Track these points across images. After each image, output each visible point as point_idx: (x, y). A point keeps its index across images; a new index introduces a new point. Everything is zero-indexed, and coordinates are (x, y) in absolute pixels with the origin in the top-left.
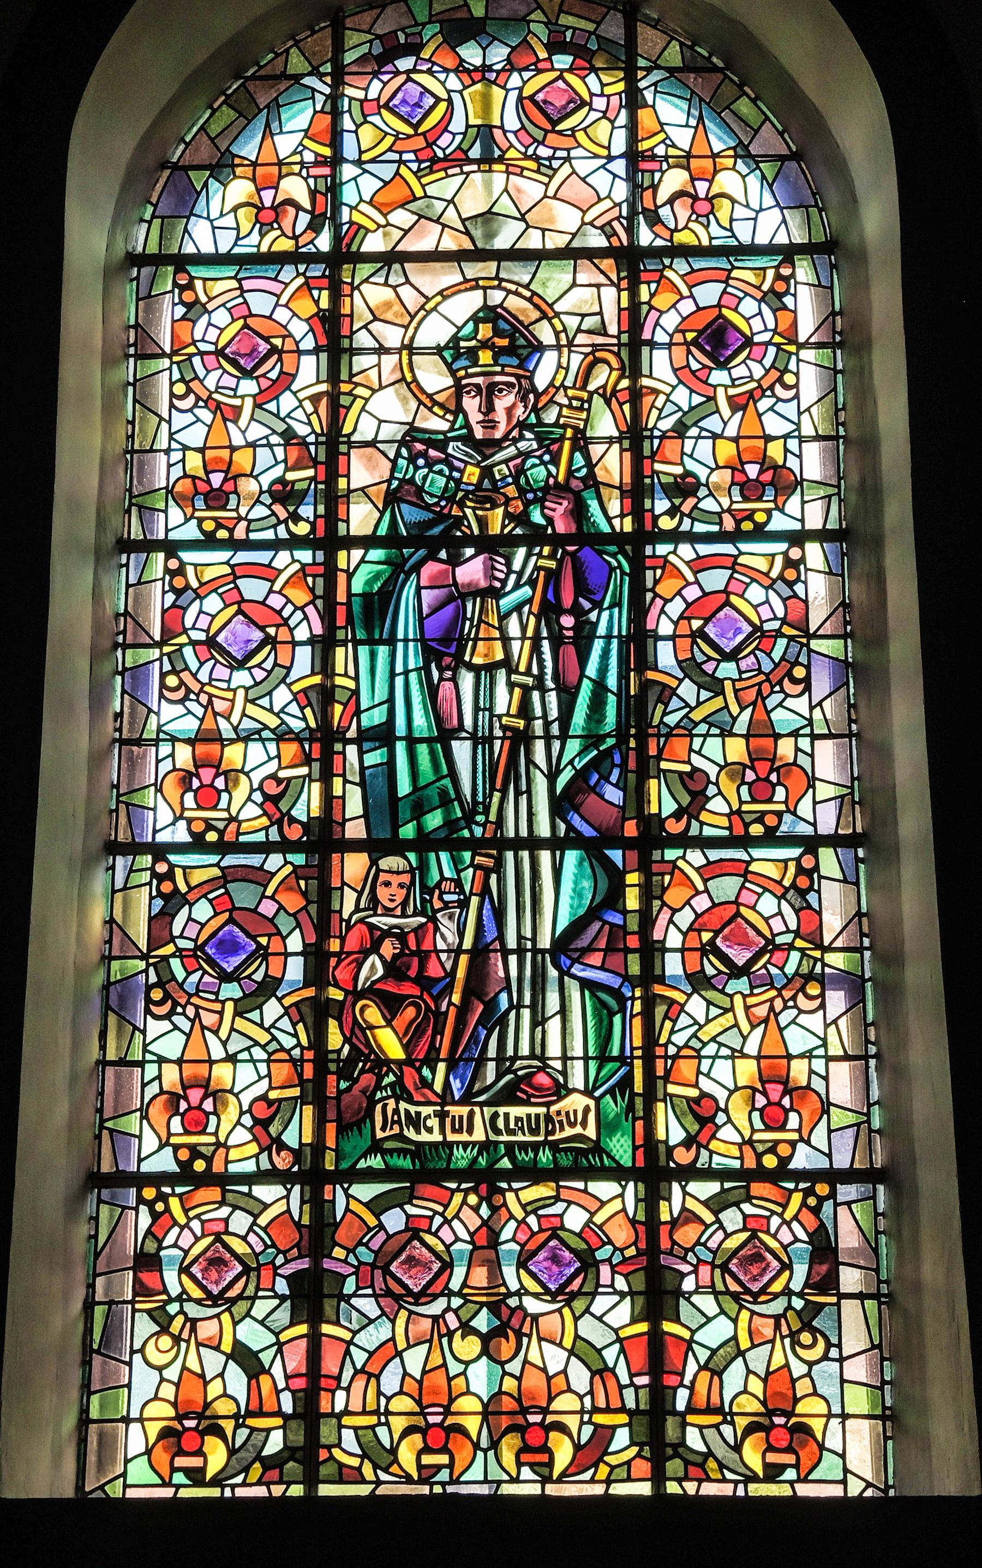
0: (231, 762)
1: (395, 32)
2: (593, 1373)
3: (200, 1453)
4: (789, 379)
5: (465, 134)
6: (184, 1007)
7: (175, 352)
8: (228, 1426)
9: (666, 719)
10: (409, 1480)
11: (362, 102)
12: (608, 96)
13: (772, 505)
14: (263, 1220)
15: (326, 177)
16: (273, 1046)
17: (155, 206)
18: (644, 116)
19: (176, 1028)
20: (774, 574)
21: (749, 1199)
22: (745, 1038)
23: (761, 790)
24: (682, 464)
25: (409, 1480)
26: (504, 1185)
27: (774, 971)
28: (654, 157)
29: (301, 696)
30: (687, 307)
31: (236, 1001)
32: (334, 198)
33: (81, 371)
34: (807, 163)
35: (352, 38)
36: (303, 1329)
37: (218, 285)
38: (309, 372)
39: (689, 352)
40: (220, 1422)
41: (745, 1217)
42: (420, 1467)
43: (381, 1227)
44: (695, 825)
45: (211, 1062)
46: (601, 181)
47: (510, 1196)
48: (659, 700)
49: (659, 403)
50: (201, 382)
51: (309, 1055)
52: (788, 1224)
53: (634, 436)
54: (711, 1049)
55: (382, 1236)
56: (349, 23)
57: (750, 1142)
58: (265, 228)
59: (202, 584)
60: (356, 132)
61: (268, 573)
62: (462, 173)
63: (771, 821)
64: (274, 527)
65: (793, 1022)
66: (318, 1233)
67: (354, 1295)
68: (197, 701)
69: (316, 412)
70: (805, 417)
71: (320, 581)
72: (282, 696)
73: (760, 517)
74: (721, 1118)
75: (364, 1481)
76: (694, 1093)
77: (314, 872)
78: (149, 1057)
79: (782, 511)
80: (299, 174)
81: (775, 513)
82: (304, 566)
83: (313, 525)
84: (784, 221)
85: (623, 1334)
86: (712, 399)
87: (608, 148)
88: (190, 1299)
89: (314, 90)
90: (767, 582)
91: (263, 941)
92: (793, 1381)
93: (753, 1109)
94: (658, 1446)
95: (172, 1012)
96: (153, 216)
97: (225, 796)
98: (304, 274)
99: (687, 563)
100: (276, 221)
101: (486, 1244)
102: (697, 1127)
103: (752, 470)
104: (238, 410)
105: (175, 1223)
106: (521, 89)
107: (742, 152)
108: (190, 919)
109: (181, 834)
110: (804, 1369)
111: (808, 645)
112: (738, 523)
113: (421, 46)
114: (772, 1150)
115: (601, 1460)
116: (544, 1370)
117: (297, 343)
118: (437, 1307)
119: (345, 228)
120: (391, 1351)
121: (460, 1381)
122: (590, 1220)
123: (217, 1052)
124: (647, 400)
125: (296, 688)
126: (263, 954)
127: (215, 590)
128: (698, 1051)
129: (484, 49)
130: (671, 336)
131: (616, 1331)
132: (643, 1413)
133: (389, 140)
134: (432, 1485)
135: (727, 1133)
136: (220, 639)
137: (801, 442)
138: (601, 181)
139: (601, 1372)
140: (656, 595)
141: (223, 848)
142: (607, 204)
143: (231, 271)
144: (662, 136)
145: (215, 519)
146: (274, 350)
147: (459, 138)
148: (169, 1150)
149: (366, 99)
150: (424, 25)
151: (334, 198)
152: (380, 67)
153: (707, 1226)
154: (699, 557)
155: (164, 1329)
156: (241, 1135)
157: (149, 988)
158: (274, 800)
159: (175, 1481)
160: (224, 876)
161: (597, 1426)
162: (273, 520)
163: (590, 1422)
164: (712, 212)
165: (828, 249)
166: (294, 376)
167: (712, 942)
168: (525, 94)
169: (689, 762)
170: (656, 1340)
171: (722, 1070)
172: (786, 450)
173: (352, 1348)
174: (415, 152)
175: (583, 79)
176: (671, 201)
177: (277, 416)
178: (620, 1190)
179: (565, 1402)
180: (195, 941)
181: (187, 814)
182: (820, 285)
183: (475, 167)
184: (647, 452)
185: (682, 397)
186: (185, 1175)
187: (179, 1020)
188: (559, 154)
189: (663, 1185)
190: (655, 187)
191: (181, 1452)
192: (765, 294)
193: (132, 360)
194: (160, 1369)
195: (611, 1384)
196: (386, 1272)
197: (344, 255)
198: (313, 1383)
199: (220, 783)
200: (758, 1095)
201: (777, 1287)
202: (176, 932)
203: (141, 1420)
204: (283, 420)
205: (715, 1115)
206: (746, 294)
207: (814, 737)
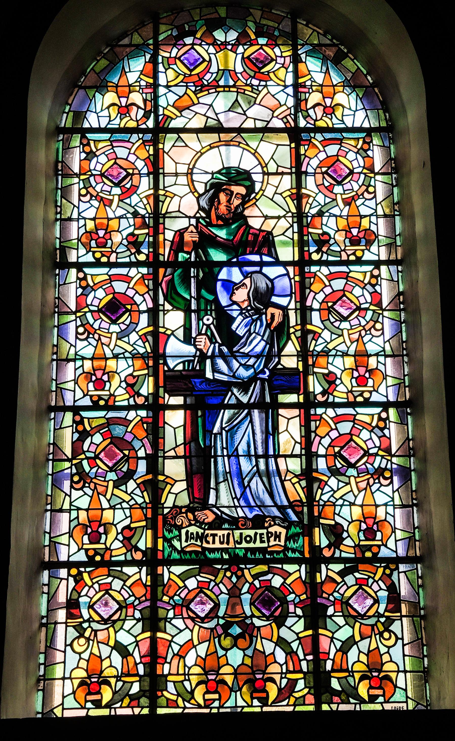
1: (183, 25)
2: (287, 654)
3: (99, 693)
5: (217, 73)
6: (89, 484)
7: (77, 311)
8: (113, 681)
9: (316, 348)
10: (199, 706)
12: (285, 57)
13: (364, 248)
14: (128, 583)
16: (132, 502)
17: (71, 105)
18: (301, 66)
19: (85, 494)
21: (358, 571)
22: (356, 497)
23: (361, 381)
24: (322, 229)
25: (199, 706)
27: (369, 466)
28: (305, 86)
29: (142, 486)
30: (322, 156)
31: (114, 481)
33: (37, 180)
34: (377, 91)
35: (163, 28)
36: (148, 634)
38: (145, 185)
39: (324, 177)
41: (357, 579)
42: (205, 700)
43: (185, 587)
44: (337, 552)
45: (103, 510)
46: (282, 97)
47: (246, 571)
49: (310, 201)
51: (149, 506)
52: (377, 582)
54: (340, 502)
55: (186, 591)
57: (351, 392)
58: (122, 116)
59: (92, 428)
60: (165, 72)
61: (126, 279)
62: (216, 92)
63: (375, 550)
65: (378, 490)
69: (148, 203)
70: (379, 206)
71: (151, 282)
72: (134, 337)
73: (359, 254)
75: (178, 707)
76: (326, 371)
79: (377, 391)
80: (139, 92)
82: (143, 275)
83: (147, 256)
84: (367, 116)
85: (301, 635)
87: (284, 81)
88: (94, 621)
90: (362, 285)
91: (126, 452)
92: (381, 655)
95: (84, 486)
96: (70, 111)
97: (108, 384)
98: (142, 139)
100: (128, 113)
101: (234, 593)
102: (328, 386)
103: (355, 232)
104: (111, 201)
105: (86, 585)
106: (243, 53)
107: (347, 84)
108: (92, 443)
109: (87, 402)
110: (386, 650)
111: (382, 314)
113: (196, 32)
114: (361, 395)
117: (139, 171)
118: (212, 624)
119: (161, 118)
120: (190, 645)
122: (284, 582)
123: (105, 505)
124: (304, 201)
125: (140, 333)
126: (127, 459)
127: (101, 287)
129: (226, 33)
130: (315, 170)
131: (297, 634)
132: (310, 673)
133: (181, 77)
134: (211, 708)
135: (341, 388)
137: (377, 218)
139: (290, 653)
140: (316, 435)
141: (108, 408)
142: (284, 108)
143: (107, 136)
144: (309, 77)
145: (101, 252)
146: (128, 174)
147: (214, 75)
149: (170, 57)
152: (177, 42)
153: (338, 584)
154: (331, 273)
155: (81, 635)
156: (117, 544)
157: (72, 476)
160: (108, 423)
161: (289, 679)
163: (285, 677)
165: (389, 131)
166: (138, 187)
167: (339, 452)
168: (245, 56)
169: (334, 520)
173: (172, 644)
174: (193, 83)
175: (273, 49)
176: (314, 107)
177: (130, 205)
178: (298, 568)
179: (273, 668)
180: (95, 453)
181: (85, 547)
182: (384, 146)
183: (222, 89)
184: (305, 223)
185: (321, 198)
186: (91, 562)
187: (87, 490)
188: (263, 83)
190: (306, 100)
191: (89, 693)
192: (359, 150)
193: (51, 462)
194: (80, 654)
195: (295, 658)
196: (188, 608)
197: (161, 130)
198: (154, 657)
199: (105, 378)
200: (362, 524)
201: (371, 613)
202: (85, 448)
203: (70, 678)
204: (133, 207)
205: (335, 380)
206: (350, 150)
207: (377, 216)
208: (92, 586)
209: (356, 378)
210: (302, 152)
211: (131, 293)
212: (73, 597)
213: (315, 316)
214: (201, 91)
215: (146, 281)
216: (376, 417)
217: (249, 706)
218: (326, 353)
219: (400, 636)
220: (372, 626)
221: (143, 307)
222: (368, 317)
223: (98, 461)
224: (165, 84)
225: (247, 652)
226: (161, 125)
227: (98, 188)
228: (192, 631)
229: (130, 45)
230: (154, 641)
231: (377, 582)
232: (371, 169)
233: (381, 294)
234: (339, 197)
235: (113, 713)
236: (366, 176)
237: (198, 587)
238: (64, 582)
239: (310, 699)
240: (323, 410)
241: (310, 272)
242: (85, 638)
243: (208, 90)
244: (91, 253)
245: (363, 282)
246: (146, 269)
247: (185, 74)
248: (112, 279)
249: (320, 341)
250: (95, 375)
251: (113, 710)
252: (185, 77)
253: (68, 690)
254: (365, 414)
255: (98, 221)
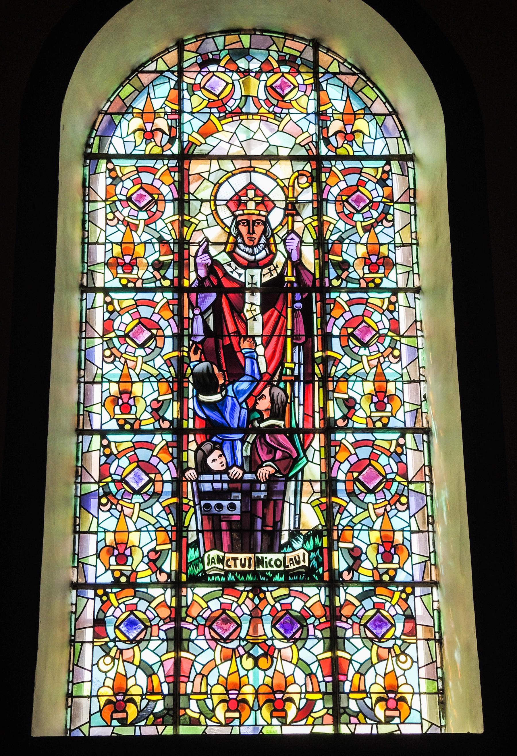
0: (138, 253)
1: (207, 53)
2: (306, 675)
3: (124, 711)
4: (390, 217)
5: (241, 99)
9: (336, 374)
11: (192, 85)
14: (153, 605)
15: (176, 119)
16: (158, 525)
20: (385, 307)
21: (376, 595)
22: (374, 522)
23: (380, 407)
24: (342, 256)
25: (222, 725)
26: (265, 589)
29: (166, 508)
32: (180, 129)
36: (172, 655)
37: (127, 166)
38: (170, 209)
39: (344, 206)
40: (133, 697)
43: (208, 607)
46: (304, 124)
47: (268, 594)
48: (333, 365)
49: (331, 228)
50: (120, 212)
52: (394, 606)
53: (320, 243)
54: (358, 527)
55: (209, 612)
56: (186, 48)
57: (370, 417)
59: (122, 309)
60: (190, 99)
61: (152, 304)
63: (385, 420)
64: (155, 282)
65: (395, 515)
66: (177, 615)
67: (196, 639)
68: (120, 361)
69: (173, 229)
70: (397, 235)
71: (176, 307)
73: (378, 281)
74: (363, 557)
76: (346, 396)
77: (176, 302)
78: (107, 241)
81: (384, 279)
83: (172, 281)
84: (387, 144)
85: (320, 657)
86: (355, 227)
89: (169, 78)
91: (152, 476)
93: (378, 553)
94: (337, 713)
95: (114, 360)
96: (96, 136)
99: (345, 302)
101: (256, 616)
104: (137, 226)
112: (367, 283)
115: (309, 715)
116: (283, 674)
117: (164, 197)
118: (234, 644)
119: (185, 144)
121: (245, 678)
122: (305, 606)
123: (132, 528)
127: (128, 312)
128: (347, 379)
129: (249, 62)
130: (336, 198)
132: (329, 694)
133: (205, 103)
135: (366, 564)
136: (127, 479)
138: (304, 124)
139: (311, 675)
141: (134, 431)
144: (330, 105)
145: (127, 278)
147: (238, 101)
148: (109, 572)
149: (195, 84)
150: (221, 51)
151: (180, 129)
153: (357, 607)
154: (350, 299)
155: (107, 654)
158: (154, 561)
159: (112, 725)
162: (154, 279)
163: (305, 698)
164: (354, 140)
170: (335, 661)
171: (364, 535)
172: (389, 250)
173: (195, 663)
175: (295, 77)
176: (335, 134)
178: (318, 592)
180: (121, 476)
181: (112, 568)
185: (341, 225)
186: (116, 583)
188: (285, 111)
189: (337, 589)
190: (328, 128)
191: (116, 711)
194: (106, 673)
195: (314, 680)
197: (185, 156)
199: (131, 402)
203: (97, 696)
204: (158, 232)
205: (361, 556)
208: (118, 607)
209: (382, 554)
210: (324, 179)
211: (156, 318)
212: (99, 617)
213: (336, 343)
214: (225, 117)
215: (171, 306)
216: (394, 443)
217: (269, 725)
218: (346, 377)
219: (415, 660)
220: (389, 649)
221: (169, 197)
222: (386, 344)
223: (127, 339)
224: (190, 110)
225: (267, 673)
226: (186, 152)
227: (126, 212)
228: (214, 651)
229: (155, 72)
230: (177, 662)
231: (394, 606)
232: (390, 197)
233: (398, 321)
234: (359, 225)
235: (138, 733)
236: (385, 204)
237: (221, 609)
238: (91, 602)
239: (329, 719)
240: (338, 294)
241: (330, 298)
242: (111, 657)
243: (232, 117)
244: (117, 279)
245: (388, 450)
246: (171, 294)
247: (209, 99)
248: (138, 170)
249: (341, 366)
250: (121, 398)
251: (138, 728)
252: (209, 102)
253: (95, 708)
254: (383, 439)
255: (124, 245)
